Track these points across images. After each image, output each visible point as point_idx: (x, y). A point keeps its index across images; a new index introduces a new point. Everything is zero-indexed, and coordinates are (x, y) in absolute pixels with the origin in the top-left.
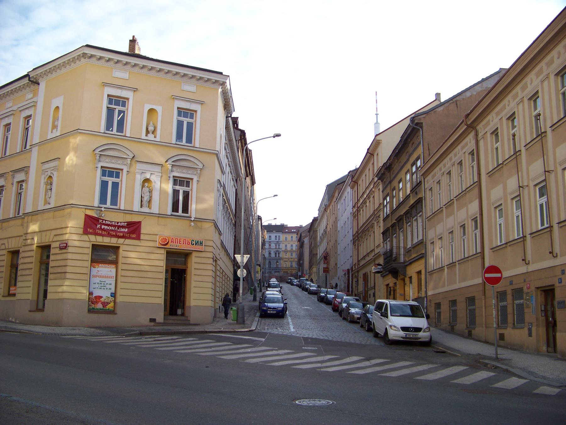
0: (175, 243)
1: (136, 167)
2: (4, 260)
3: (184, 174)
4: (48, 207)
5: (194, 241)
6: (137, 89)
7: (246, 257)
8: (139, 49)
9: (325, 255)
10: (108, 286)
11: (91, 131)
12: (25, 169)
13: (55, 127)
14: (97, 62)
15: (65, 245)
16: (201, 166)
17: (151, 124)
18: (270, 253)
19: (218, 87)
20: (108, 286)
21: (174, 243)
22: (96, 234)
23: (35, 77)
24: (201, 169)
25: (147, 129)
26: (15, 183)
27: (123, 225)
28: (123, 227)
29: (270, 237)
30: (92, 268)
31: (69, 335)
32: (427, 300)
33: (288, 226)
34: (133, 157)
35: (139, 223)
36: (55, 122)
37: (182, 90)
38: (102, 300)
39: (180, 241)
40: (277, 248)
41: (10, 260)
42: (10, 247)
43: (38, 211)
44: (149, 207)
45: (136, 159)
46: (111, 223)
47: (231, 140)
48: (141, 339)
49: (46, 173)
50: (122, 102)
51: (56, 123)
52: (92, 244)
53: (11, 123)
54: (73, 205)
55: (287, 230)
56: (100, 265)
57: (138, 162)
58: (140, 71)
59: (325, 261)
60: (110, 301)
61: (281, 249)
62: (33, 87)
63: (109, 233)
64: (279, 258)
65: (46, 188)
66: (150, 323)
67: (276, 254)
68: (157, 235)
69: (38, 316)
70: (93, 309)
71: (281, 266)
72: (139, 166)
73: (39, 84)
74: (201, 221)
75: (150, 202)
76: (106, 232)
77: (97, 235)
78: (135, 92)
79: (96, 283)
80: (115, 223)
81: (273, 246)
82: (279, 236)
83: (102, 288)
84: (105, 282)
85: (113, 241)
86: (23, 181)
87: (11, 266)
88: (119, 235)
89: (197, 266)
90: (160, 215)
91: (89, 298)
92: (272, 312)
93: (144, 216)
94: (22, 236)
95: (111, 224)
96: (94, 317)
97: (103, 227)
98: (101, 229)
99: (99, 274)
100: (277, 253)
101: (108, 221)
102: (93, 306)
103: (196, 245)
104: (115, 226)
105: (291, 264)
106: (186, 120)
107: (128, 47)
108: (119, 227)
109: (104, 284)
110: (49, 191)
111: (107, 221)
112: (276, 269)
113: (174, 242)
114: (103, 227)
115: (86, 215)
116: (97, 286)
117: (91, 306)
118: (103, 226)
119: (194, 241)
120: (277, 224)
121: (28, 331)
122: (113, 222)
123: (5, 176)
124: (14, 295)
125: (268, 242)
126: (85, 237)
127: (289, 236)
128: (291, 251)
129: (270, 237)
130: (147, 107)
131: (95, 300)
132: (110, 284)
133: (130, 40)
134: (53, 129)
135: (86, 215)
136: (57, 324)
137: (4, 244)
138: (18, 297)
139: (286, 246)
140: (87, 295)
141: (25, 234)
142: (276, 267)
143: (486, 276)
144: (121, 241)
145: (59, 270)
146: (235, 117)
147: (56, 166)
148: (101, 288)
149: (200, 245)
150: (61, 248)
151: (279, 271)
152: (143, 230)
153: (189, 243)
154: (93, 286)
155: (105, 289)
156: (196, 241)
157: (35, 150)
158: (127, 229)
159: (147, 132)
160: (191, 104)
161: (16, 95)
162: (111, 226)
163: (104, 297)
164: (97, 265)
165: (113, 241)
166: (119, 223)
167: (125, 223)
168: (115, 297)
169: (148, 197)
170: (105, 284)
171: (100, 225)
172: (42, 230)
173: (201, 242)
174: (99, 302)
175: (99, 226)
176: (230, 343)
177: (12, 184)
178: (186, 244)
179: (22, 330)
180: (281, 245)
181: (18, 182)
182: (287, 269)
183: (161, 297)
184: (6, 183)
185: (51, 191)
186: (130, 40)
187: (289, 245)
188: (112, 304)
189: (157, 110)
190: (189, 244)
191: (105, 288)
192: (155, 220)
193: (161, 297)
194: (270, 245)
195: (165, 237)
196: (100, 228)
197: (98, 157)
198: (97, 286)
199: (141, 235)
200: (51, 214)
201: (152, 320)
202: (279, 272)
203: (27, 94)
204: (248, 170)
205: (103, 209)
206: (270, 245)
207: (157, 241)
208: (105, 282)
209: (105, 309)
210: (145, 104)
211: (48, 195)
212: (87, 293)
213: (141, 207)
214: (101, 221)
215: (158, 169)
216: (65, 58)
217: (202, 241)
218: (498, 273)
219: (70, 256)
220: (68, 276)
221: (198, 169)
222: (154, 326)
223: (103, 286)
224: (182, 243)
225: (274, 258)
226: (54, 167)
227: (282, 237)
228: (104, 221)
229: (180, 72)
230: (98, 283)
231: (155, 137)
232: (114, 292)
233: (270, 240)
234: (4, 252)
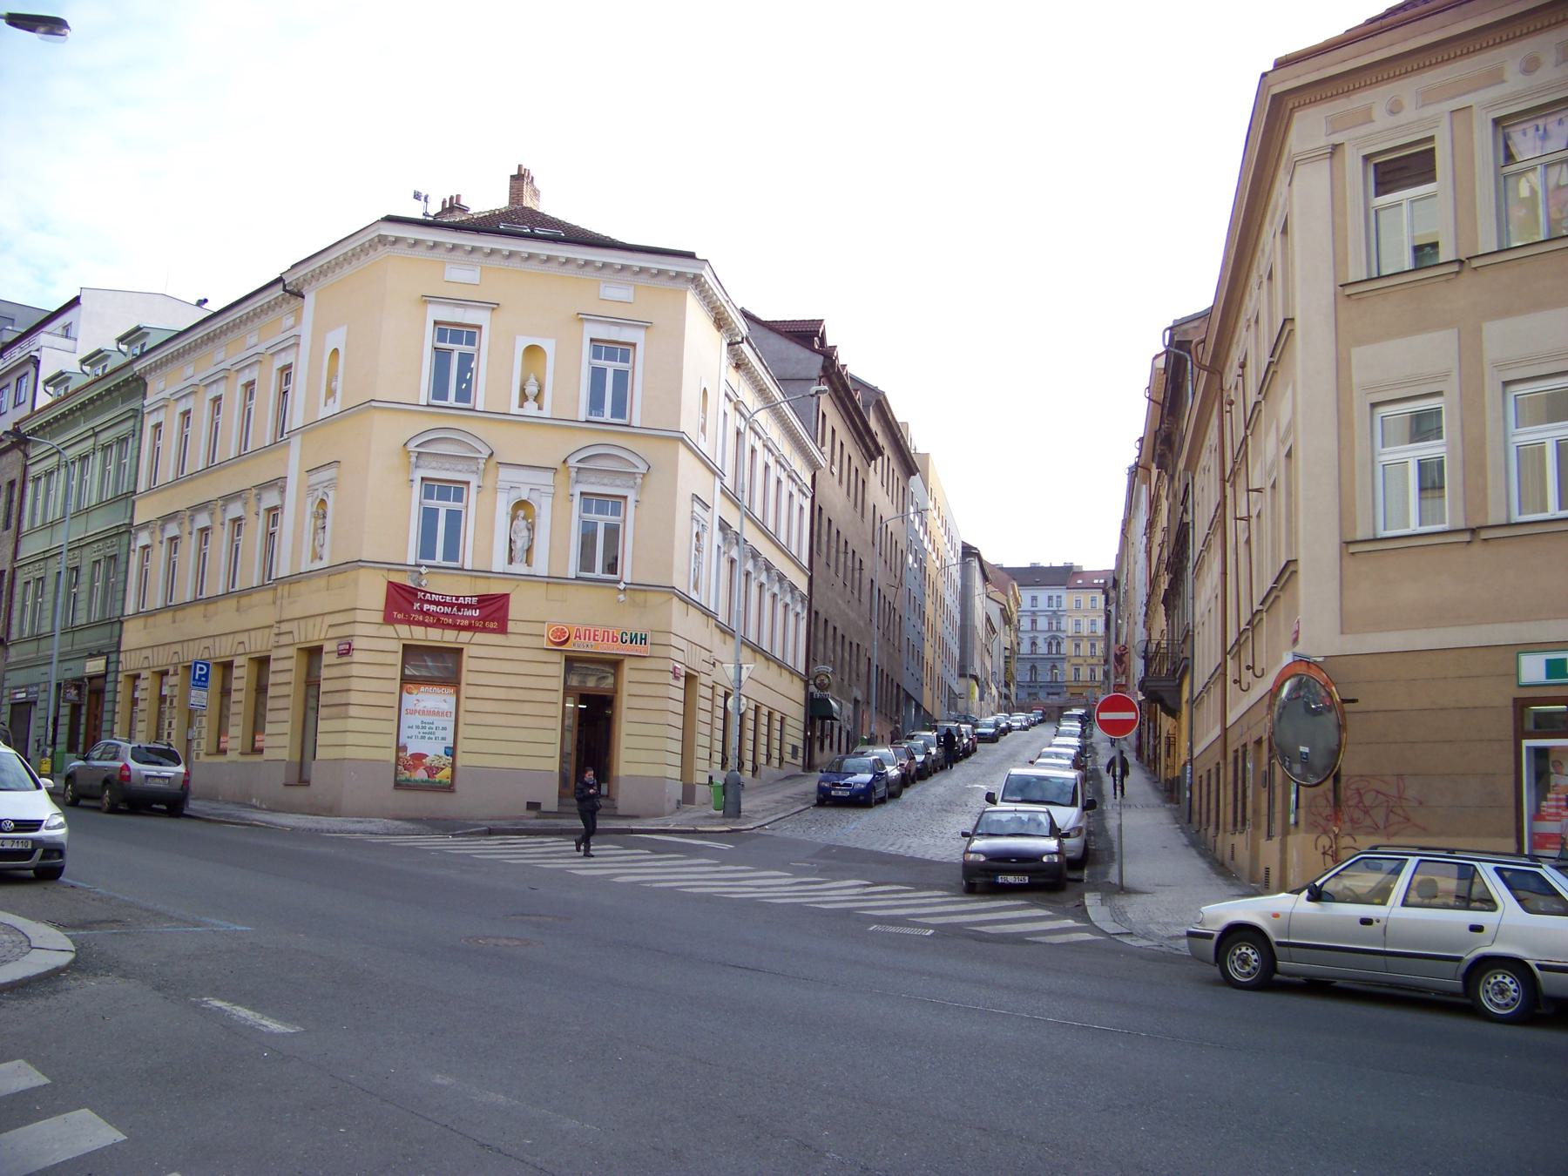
0: (585, 639)
1: (497, 477)
2: (243, 678)
4: (318, 565)
5: (627, 635)
6: (498, 304)
7: (747, 668)
8: (536, 193)
9: (1118, 653)
10: (440, 734)
12: (278, 484)
13: (331, 393)
14: (410, 251)
15: (347, 647)
16: (643, 468)
17: (532, 380)
18: (1034, 644)
20: (440, 734)
22: (410, 622)
23: (294, 283)
24: (644, 474)
25: (523, 390)
26: (262, 513)
28: (469, 606)
29: (1034, 599)
30: (405, 695)
31: (342, 833)
32: (1192, 769)
33: (1084, 569)
34: (492, 454)
35: (506, 596)
36: (331, 383)
38: (427, 761)
39: (595, 635)
40: (1054, 628)
41: (304, 671)
42: (253, 649)
43: (300, 573)
44: (528, 562)
45: (496, 458)
47: (765, 390)
48: (479, 840)
49: (316, 493)
50: (469, 334)
51: (334, 384)
52: (404, 645)
53: (254, 380)
54: (358, 563)
55: (1080, 582)
56: (422, 689)
59: (1119, 667)
61: (1064, 631)
62: (294, 302)
63: (439, 620)
64: (1058, 656)
65: (315, 524)
67: (1050, 644)
68: (544, 622)
69: (299, 793)
71: (1065, 679)
72: (505, 473)
73: (303, 297)
74: (645, 591)
75: (529, 550)
77: (413, 625)
81: (1042, 623)
82: (1059, 597)
83: (427, 736)
85: (448, 637)
86: (276, 508)
87: (256, 690)
88: (462, 624)
89: (635, 689)
90: (551, 580)
91: (398, 758)
92: (840, 793)
93: (516, 583)
94: (272, 626)
96: (403, 795)
97: (426, 607)
98: (421, 611)
99: (420, 706)
100: (1054, 643)
101: (436, 594)
102: (407, 774)
103: (631, 643)
104: (451, 605)
105: (1092, 671)
106: (611, 367)
107: (508, 193)
108: (460, 606)
110: (319, 531)
111: (433, 596)
112: (1052, 687)
113: (582, 637)
114: (426, 607)
115: (390, 582)
116: (414, 732)
117: (402, 774)
118: (425, 606)
119: (627, 635)
120: (1053, 565)
121: (267, 823)
123: (243, 496)
124: (261, 751)
125: (1029, 614)
126: (389, 630)
127: (1085, 597)
128: (1092, 639)
129: (1034, 599)
130: (523, 342)
132: (444, 729)
133: (511, 176)
134: (327, 398)
136: (331, 811)
137: (243, 643)
138: (267, 754)
139: (1078, 623)
141: (277, 622)
142: (1050, 682)
143: (1134, 713)
144: (465, 636)
145: (337, 698)
146: (797, 319)
147: (331, 480)
148: (423, 738)
149: (641, 643)
150: (341, 655)
151: (1059, 691)
152: (513, 612)
153: (615, 639)
154: (405, 732)
155: (432, 739)
157: (296, 442)
158: (478, 611)
159: (524, 397)
161: (266, 319)
162: (444, 604)
165: (448, 637)
167: (474, 599)
168: (453, 756)
172: (506, 571)
174: (420, 766)
175: (417, 605)
176: (647, 852)
177: (257, 514)
179: (253, 820)
180: (1063, 620)
181: (269, 510)
182: (1082, 686)
183: (553, 757)
184: (245, 512)
185: (324, 532)
186: (511, 176)
187: (1085, 623)
188: (447, 771)
189: (545, 349)
190: (616, 642)
192: (541, 589)
193: (553, 757)
194: (1034, 622)
197: (413, 459)
198: (414, 732)
199: (510, 622)
200: (322, 582)
201: (533, 806)
202: (1058, 694)
203: (284, 318)
204: (870, 444)
205: (423, 570)
206: (1034, 622)
207: (543, 636)
208: (433, 723)
210: (517, 337)
211: (319, 540)
213: (511, 560)
214: (420, 595)
216: (346, 247)
217: (646, 635)
218: (1130, 711)
219: (355, 670)
220: (353, 711)
221: (637, 475)
222: (537, 818)
223: (427, 732)
224: (600, 640)
225: (1045, 656)
226: (328, 480)
227: (1068, 598)
228: (428, 595)
229: (594, 261)
230: (418, 727)
231: (540, 408)
232: (452, 746)
233: (1033, 609)
234: (292, 651)
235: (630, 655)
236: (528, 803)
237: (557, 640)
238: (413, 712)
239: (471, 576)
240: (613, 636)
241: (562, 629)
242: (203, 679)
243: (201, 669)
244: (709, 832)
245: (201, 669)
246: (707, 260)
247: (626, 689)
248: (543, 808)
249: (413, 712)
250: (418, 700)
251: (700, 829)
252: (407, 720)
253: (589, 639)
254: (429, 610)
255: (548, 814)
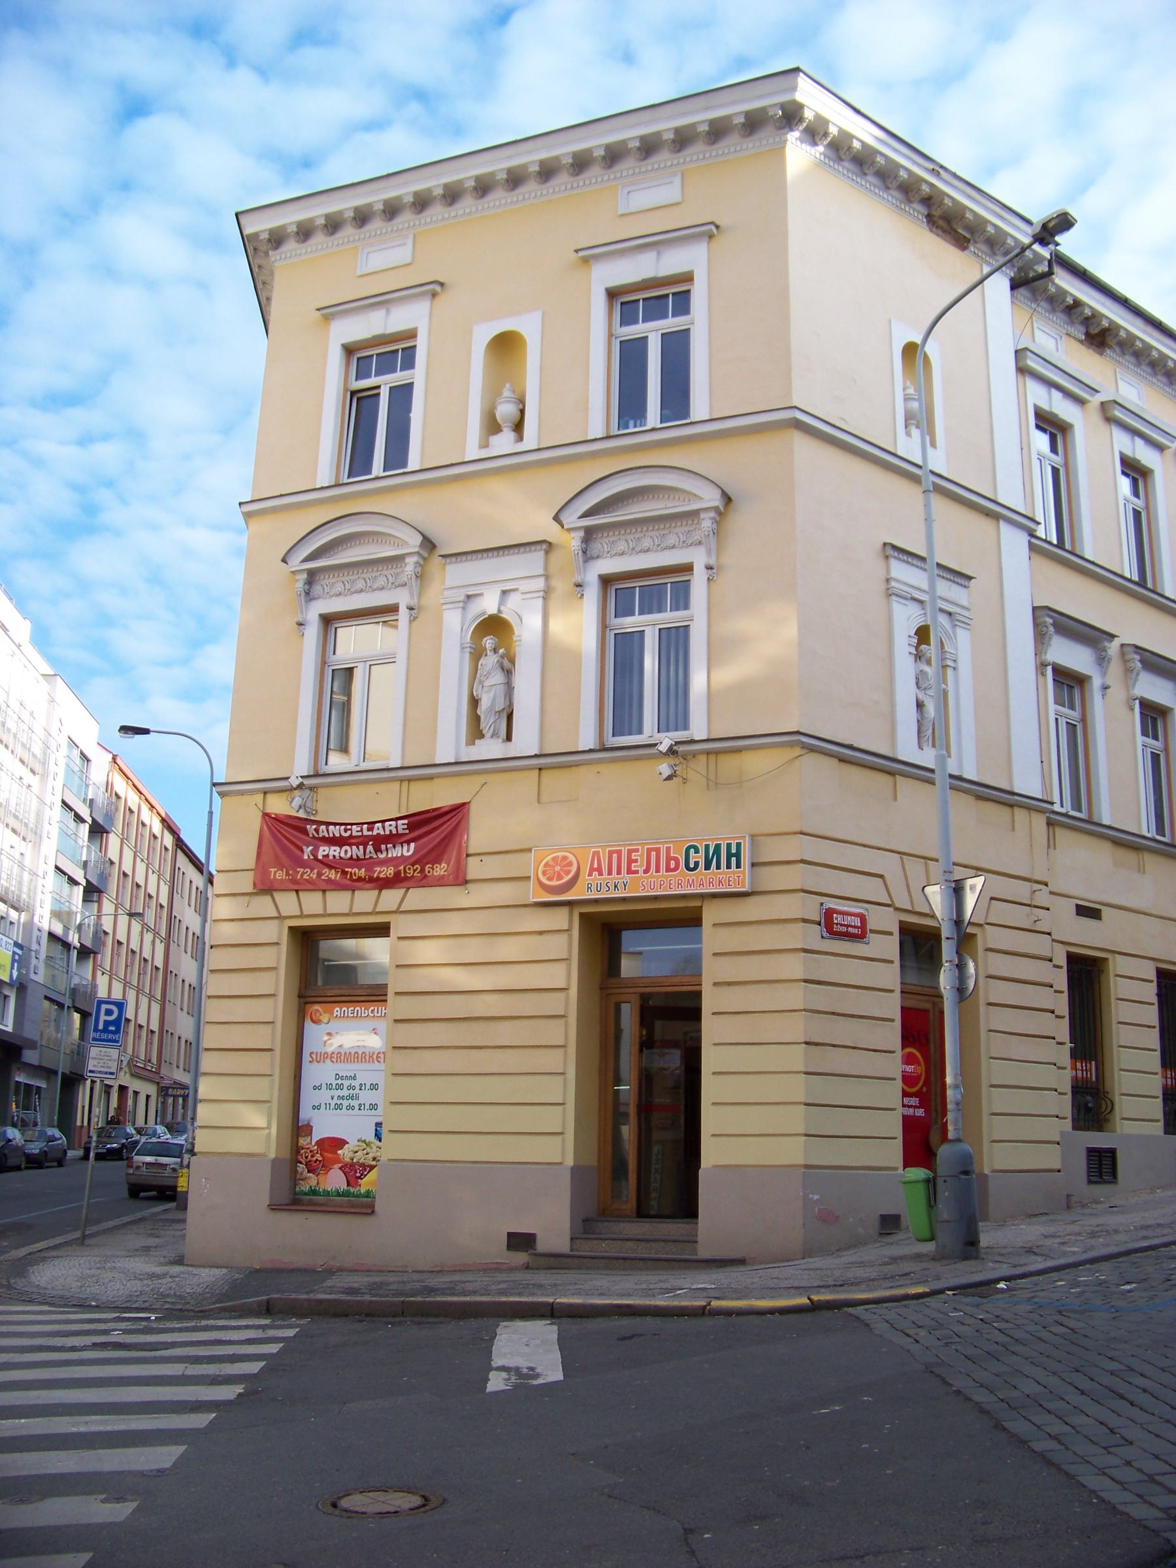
0: (610, 873)
3: (674, 551)
5: (697, 851)
11: (281, 495)
19: (777, 139)
20: (367, 1097)
21: (605, 876)
22: (297, 887)
27: (394, 832)
28: (393, 839)
30: (309, 1025)
37: (622, 215)
39: (630, 861)
46: (346, 831)
56: (337, 1010)
57: (448, 560)
58: (453, 214)
60: (374, 1159)
66: (512, 1254)
70: (314, 1192)
72: (458, 575)
76: (333, 871)
78: (438, 299)
79: (324, 1086)
80: (362, 831)
83: (345, 1103)
84: (354, 1078)
88: (382, 876)
93: (482, 779)
95: (348, 833)
97: (323, 850)
101: (335, 824)
102: (312, 1180)
103: (707, 867)
104: (363, 841)
108: (379, 842)
109: (351, 1087)
111: (331, 828)
113: (605, 870)
116: (324, 1096)
119: (697, 851)
122: (354, 827)
126: (263, 906)
131: (318, 1157)
132: (374, 1087)
135: (266, 815)
140: (269, 1134)
144: (391, 898)
148: (338, 1107)
149: (729, 867)
154: (309, 1097)
155: (353, 1108)
156: (707, 847)
159: (492, 426)
160: (659, 254)
163: (353, 1144)
164: (325, 1013)
166: (377, 825)
167: (400, 822)
169: (501, 690)
170: (354, 1088)
171: (311, 848)
173: (734, 851)
178: (658, 871)
191: (355, 1103)
195: (560, 854)
196: (312, 857)
201: (520, 1241)
208: (354, 1078)
209: (354, 1196)
212: (269, 1127)
213: (476, 732)
215: (534, 561)
217: (738, 845)
222: (527, 1267)
224: (641, 870)
228: (323, 827)
230: (329, 1087)
235: (714, 896)
236: (510, 1235)
237: (555, 883)
238: (323, 1057)
239: (402, 780)
240: (669, 859)
241: (565, 858)
242: (112, 1028)
243: (109, 1012)
244: (740, 1313)
245: (109, 1012)
246: (797, 70)
247: (712, 971)
248: (542, 1246)
249: (323, 1057)
250: (329, 1034)
251: (715, 1303)
252: (314, 1074)
253: (619, 872)
254: (327, 856)
255: (555, 1261)
